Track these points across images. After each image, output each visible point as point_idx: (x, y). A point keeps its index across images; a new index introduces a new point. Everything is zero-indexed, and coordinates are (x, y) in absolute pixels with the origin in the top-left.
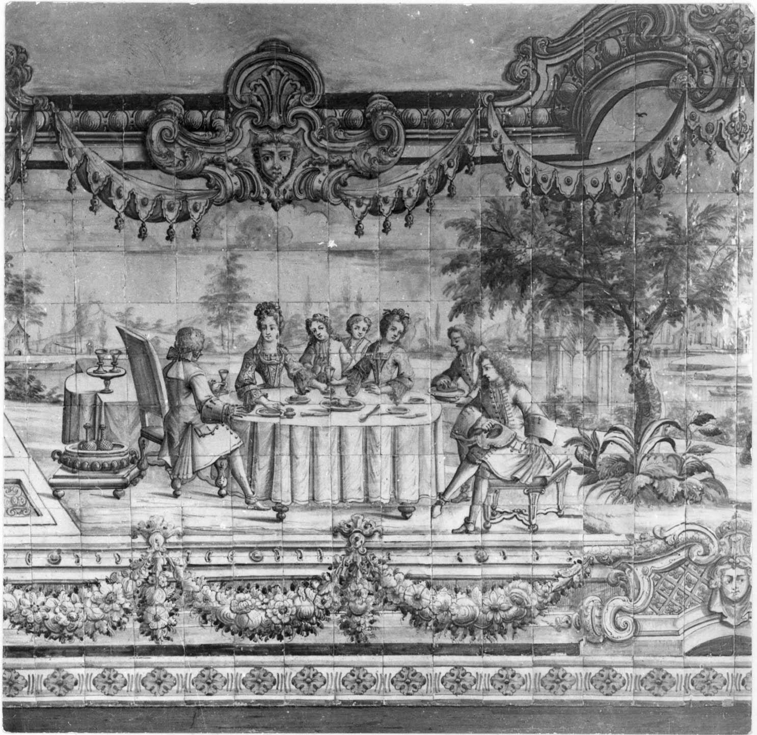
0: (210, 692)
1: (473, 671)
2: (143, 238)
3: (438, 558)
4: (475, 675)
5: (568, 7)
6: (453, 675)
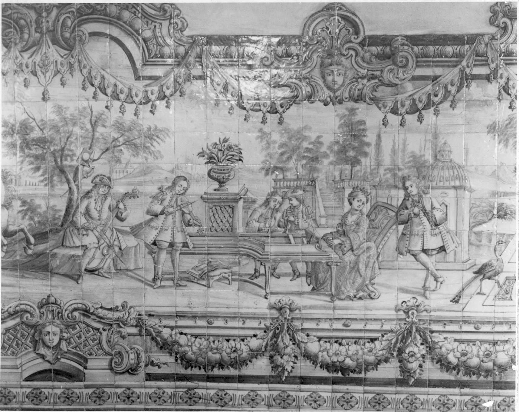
0: (38, 403)
1: (77, 391)
2: (403, 126)
3: (466, 328)
4: (295, 397)
5: (324, 3)
6: (33, 393)
